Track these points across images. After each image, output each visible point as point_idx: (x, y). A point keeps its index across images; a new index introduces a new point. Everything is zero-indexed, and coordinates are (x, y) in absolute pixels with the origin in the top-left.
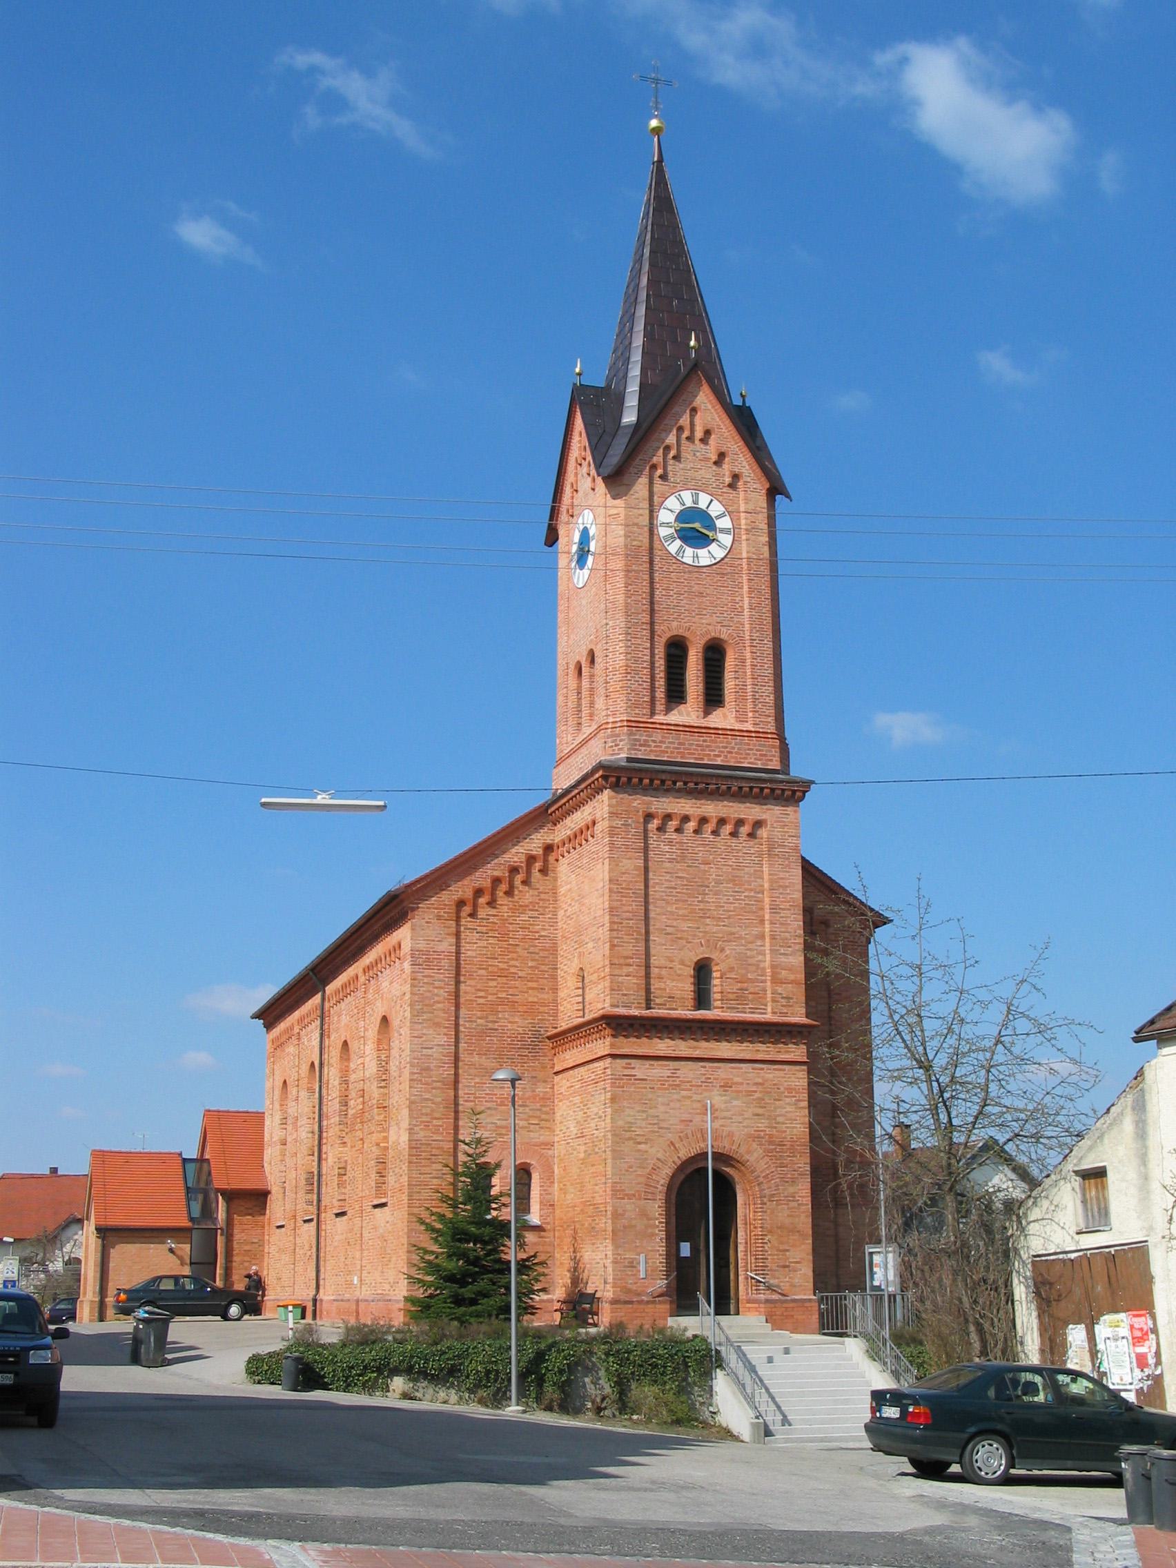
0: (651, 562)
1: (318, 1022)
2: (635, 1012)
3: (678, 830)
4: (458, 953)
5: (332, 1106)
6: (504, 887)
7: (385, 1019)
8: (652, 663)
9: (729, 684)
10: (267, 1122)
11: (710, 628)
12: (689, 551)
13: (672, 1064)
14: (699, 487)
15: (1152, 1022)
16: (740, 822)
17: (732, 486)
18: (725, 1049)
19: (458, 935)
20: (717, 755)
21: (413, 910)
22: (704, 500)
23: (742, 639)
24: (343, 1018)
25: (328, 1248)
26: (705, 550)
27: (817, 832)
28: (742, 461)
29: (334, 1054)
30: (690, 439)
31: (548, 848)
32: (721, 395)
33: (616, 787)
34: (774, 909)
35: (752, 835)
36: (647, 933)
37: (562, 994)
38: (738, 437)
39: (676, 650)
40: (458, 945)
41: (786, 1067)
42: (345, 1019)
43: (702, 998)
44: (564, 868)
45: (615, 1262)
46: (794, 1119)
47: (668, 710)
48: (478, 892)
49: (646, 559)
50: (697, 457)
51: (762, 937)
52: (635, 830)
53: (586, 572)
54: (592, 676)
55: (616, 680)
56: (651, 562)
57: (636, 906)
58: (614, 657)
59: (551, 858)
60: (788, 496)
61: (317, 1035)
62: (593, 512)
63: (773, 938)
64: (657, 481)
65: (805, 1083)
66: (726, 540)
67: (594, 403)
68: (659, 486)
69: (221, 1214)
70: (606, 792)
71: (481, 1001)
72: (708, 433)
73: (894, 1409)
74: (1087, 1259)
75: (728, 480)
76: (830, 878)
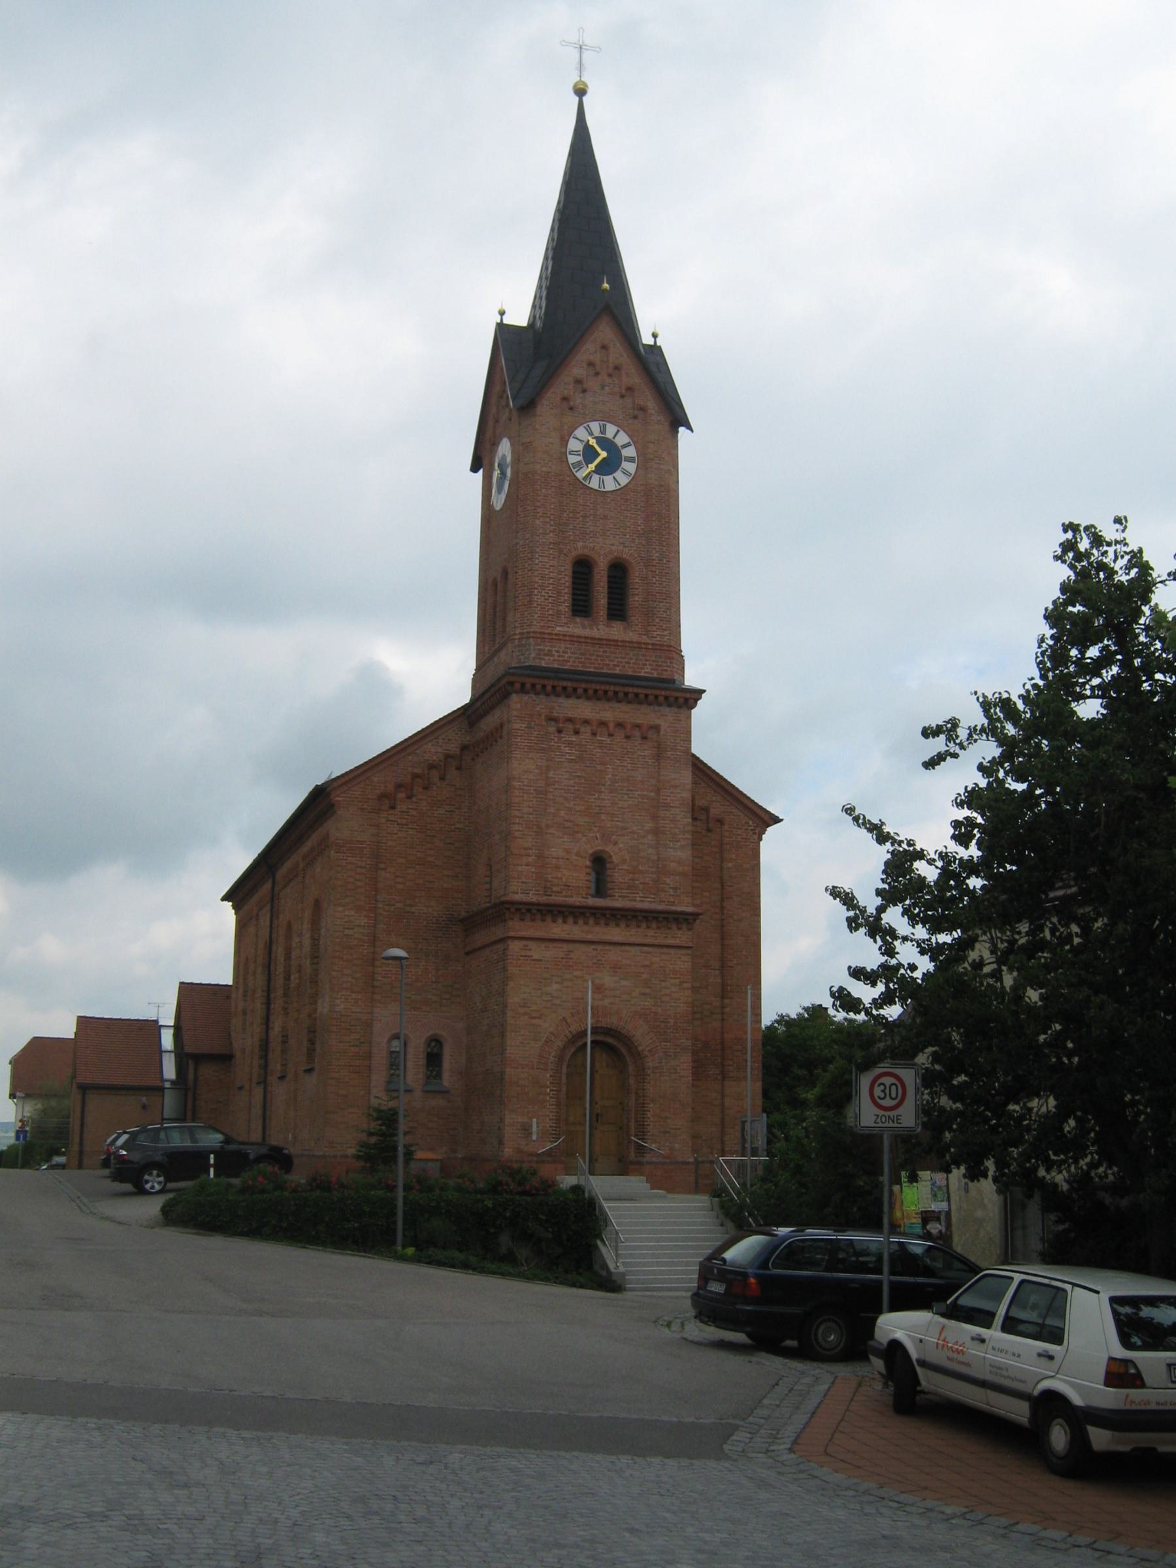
1: (269, 906)
11: (614, 548)
13: (566, 947)
18: (616, 933)
26: (611, 477)
41: (672, 951)
43: (600, 889)
60: (689, 428)
70: (514, 697)
71: (400, 887)
73: (895, 1017)
76: (725, 780)
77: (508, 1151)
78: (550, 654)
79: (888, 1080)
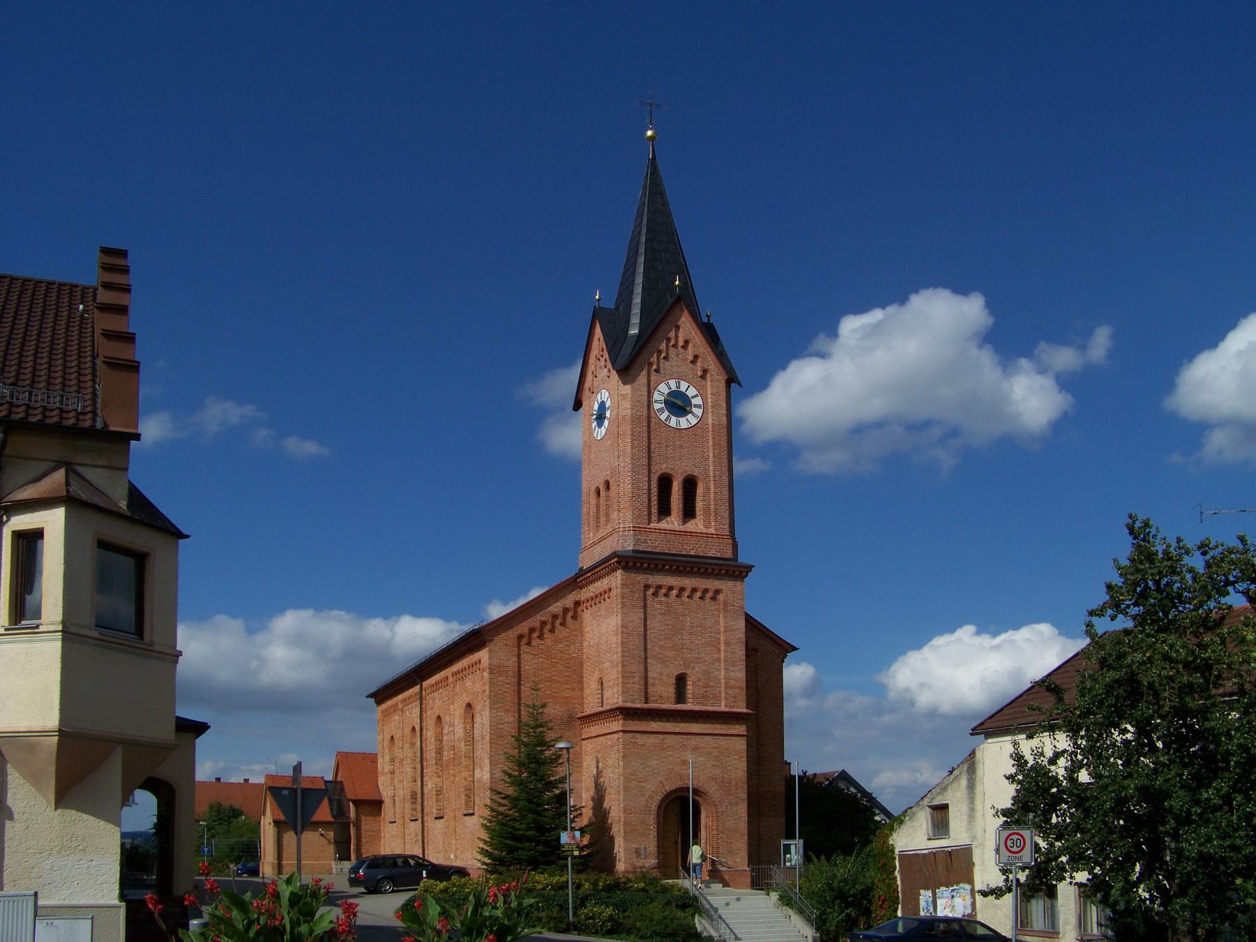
0: (649, 426)
2: (639, 706)
3: (666, 595)
4: (519, 667)
5: (430, 754)
6: (549, 627)
7: (469, 706)
8: (649, 490)
9: (699, 505)
10: (380, 761)
12: (674, 419)
13: (661, 736)
14: (680, 378)
15: (982, 724)
16: (706, 591)
17: (703, 377)
18: (695, 727)
19: (519, 656)
20: (691, 548)
21: (490, 641)
22: (684, 386)
23: (708, 476)
24: (436, 702)
25: (429, 837)
27: (760, 598)
28: (711, 362)
29: (430, 724)
30: (675, 346)
31: (577, 603)
32: (695, 316)
33: (625, 568)
34: (727, 643)
35: (713, 598)
36: (646, 658)
37: (587, 692)
38: (707, 345)
39: (665, 482)
40: (519, 663)
42: (438, 703)
43: (680, 697)
44: (587, 616)
45: (626, 850)
46: (738, 768)
47: (659, 520)
48: (532, 630)
49: (645, 424)
50: (677, 361)
51: (719, 660)
52: (638, 595)
53: (603, 430)
54: (608, 497)
55: (625, 502)
56: (649, 426)
57: (638, 641)
58: (624, 487)
59: (579, 610)
61: (418, 709)
62: (608, 392)
63: (726, 661)
64: (653, 373)
65: (745, 747)
66: (699, 412)
67: (610, 320)
68: (654, 377)
69: (352, 813)
70: (619, 572)
72: (687, 342)
74: (934, 855)
75: (700, 373)
77: (922, 913)
78: (645, 541)
79: (1015, 837)
